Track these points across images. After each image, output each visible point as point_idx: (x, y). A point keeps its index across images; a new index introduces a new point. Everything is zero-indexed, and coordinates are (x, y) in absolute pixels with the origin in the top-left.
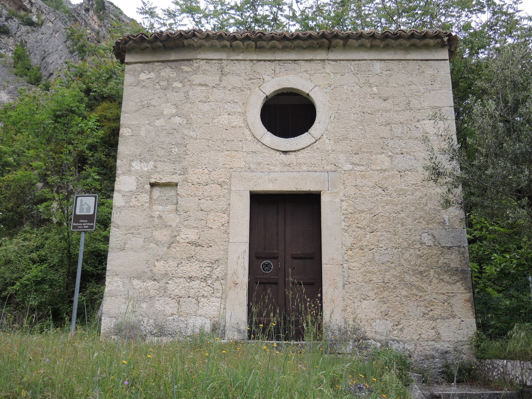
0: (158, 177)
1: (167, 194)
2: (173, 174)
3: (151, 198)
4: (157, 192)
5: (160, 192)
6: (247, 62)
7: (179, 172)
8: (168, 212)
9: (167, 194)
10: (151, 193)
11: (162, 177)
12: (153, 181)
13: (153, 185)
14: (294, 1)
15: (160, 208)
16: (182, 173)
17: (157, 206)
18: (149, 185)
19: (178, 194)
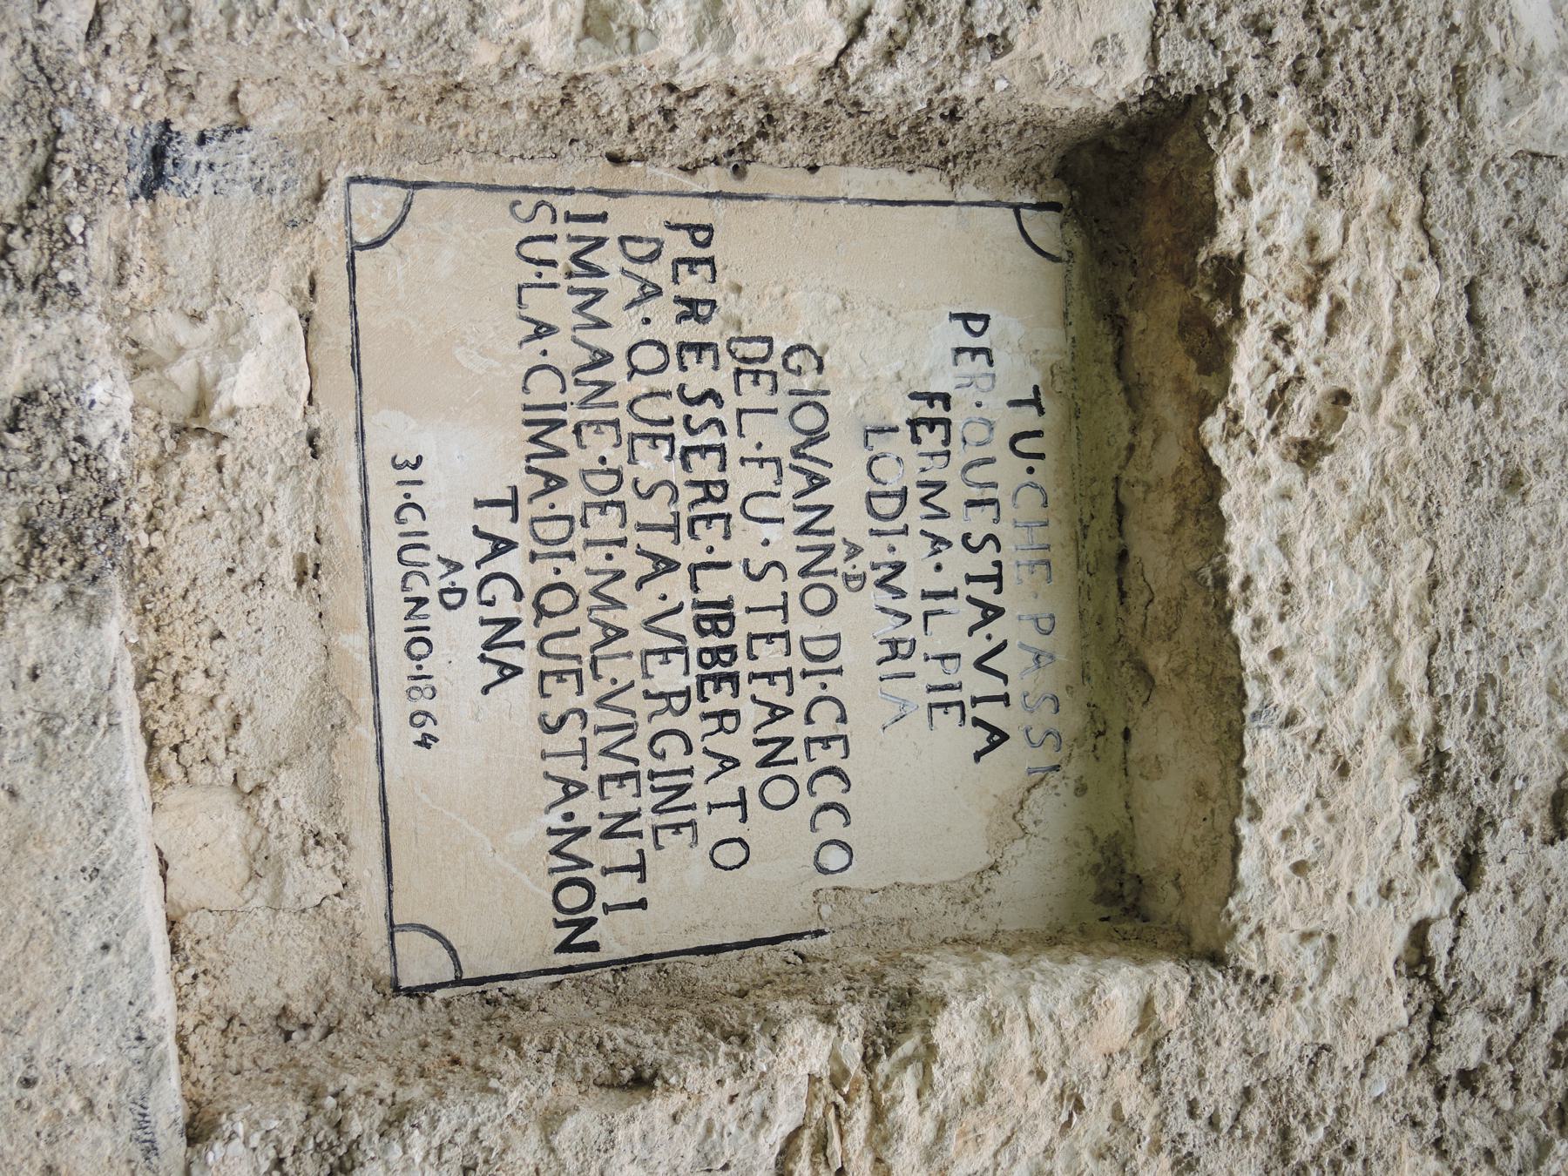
0: (1355, 359)
1: (861, 620)
2: (1435, 771)
3: (751, 132)
4: (907, 307)
5: (932, 414)
6: (1485, 307)
7: (1491, 946)
8: (326, 717)
9: (861, 620)
10: (898, 142)
11: (1361, 449)
12: (1267, 202)
13: (1125, 203)
14: (1467, 1172)
15: (466, 458)
16: (1469, 1038)
17: (494, 356)
18: (1120, 81)
19: (901, 1017)
